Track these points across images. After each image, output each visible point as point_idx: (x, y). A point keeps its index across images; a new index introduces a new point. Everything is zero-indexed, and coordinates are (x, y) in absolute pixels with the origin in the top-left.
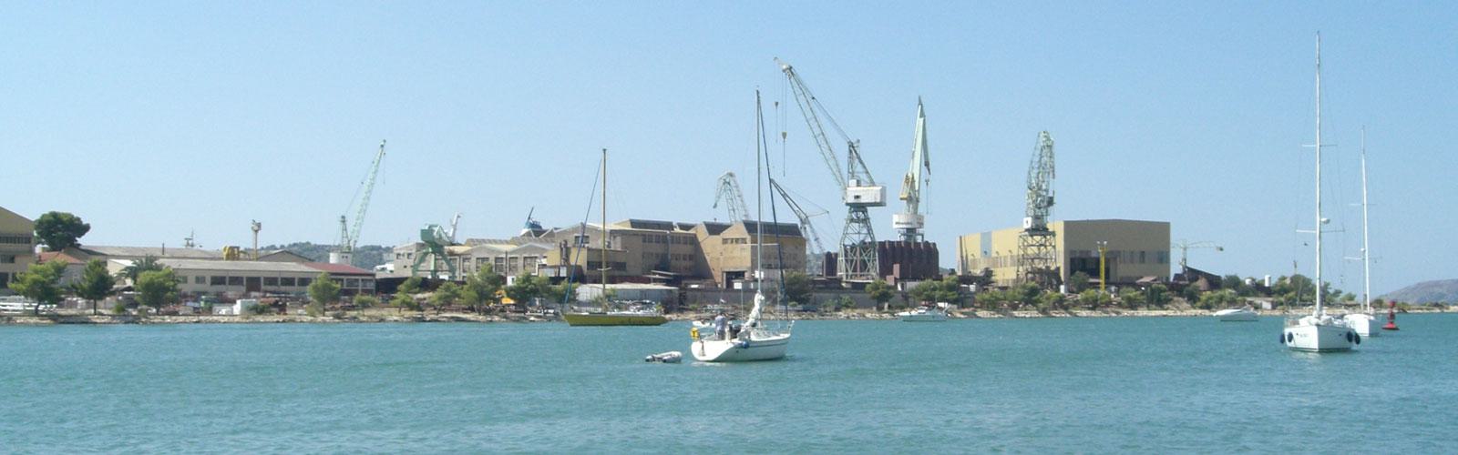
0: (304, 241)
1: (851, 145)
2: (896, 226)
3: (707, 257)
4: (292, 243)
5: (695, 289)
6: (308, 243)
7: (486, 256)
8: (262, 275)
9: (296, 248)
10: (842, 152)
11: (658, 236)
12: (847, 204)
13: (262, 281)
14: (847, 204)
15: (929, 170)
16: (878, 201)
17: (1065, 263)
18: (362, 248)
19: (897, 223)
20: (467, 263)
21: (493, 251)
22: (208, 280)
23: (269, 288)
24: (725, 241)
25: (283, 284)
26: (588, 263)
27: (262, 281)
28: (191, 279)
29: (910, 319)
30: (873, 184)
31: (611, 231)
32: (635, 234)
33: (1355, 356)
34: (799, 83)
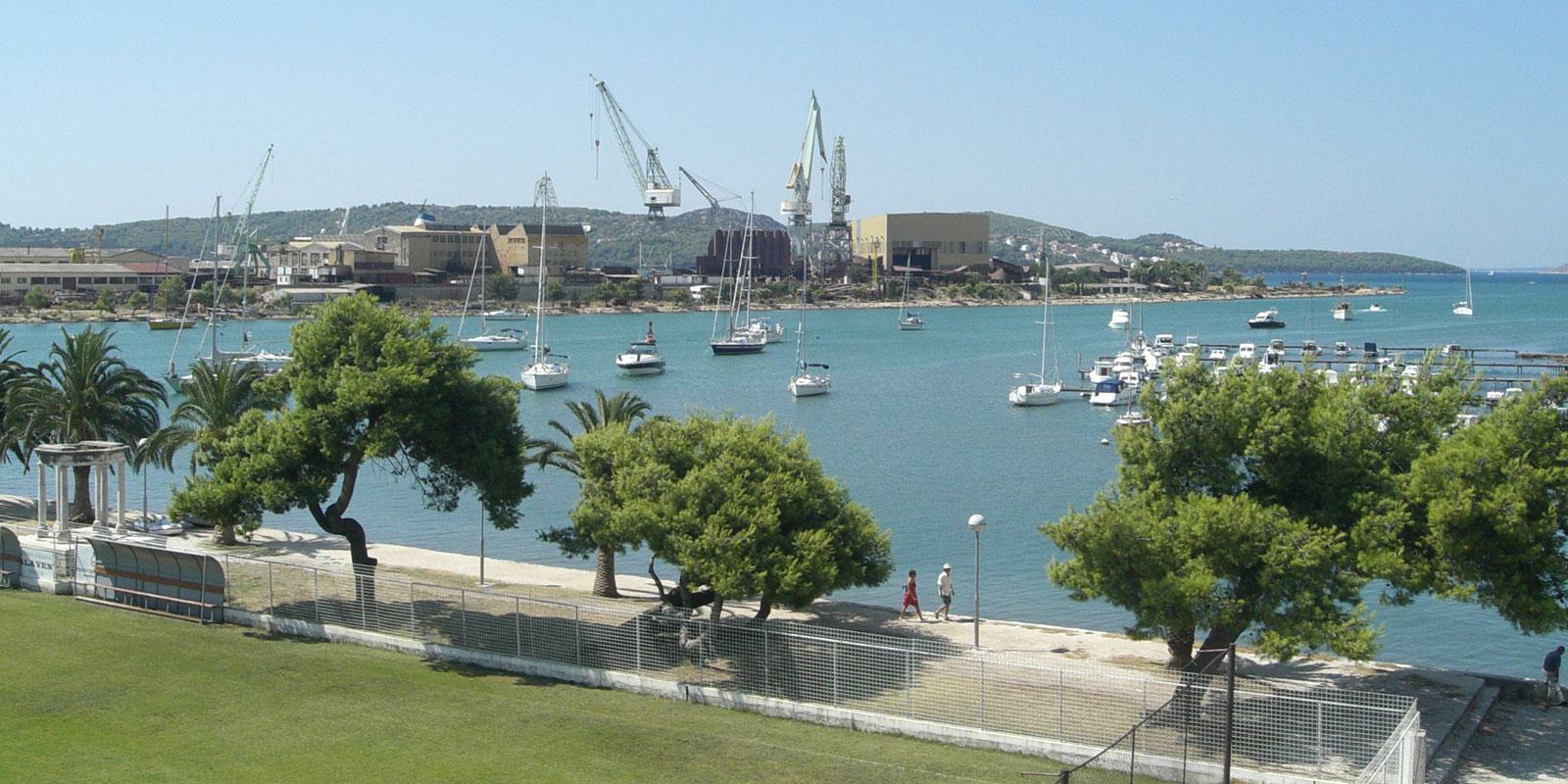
0: (397, 201)
1: (651, 153)
2: (783, 213)
3: (498, 255)
4: (384, 203)
5: (453, 285)
6: (401, 203)
7: (317, 252)
8: (77, 276)
9: (387, 208)
10: (643, 157)
11: (450, 236)
12: (646, 205)
13: (77, 280)
14: (646, 205)
15: (825, 159)
16: (670, 202)
17: (888, 253)
18: (457, 208)
19: (784, 210)
20: (304, 258)
21: (323, 248)
22: (29, 281)
23: (83, 286)
24: (510, 240)
25: (96, 282)
26: (356, 264)
27: (77, 280)
28: (14, 281)
29: (489, 319)
30: (668, 187)
31: (403, 233)
32: (428, 235)
33: (763, 355)
34: (610, 97)
